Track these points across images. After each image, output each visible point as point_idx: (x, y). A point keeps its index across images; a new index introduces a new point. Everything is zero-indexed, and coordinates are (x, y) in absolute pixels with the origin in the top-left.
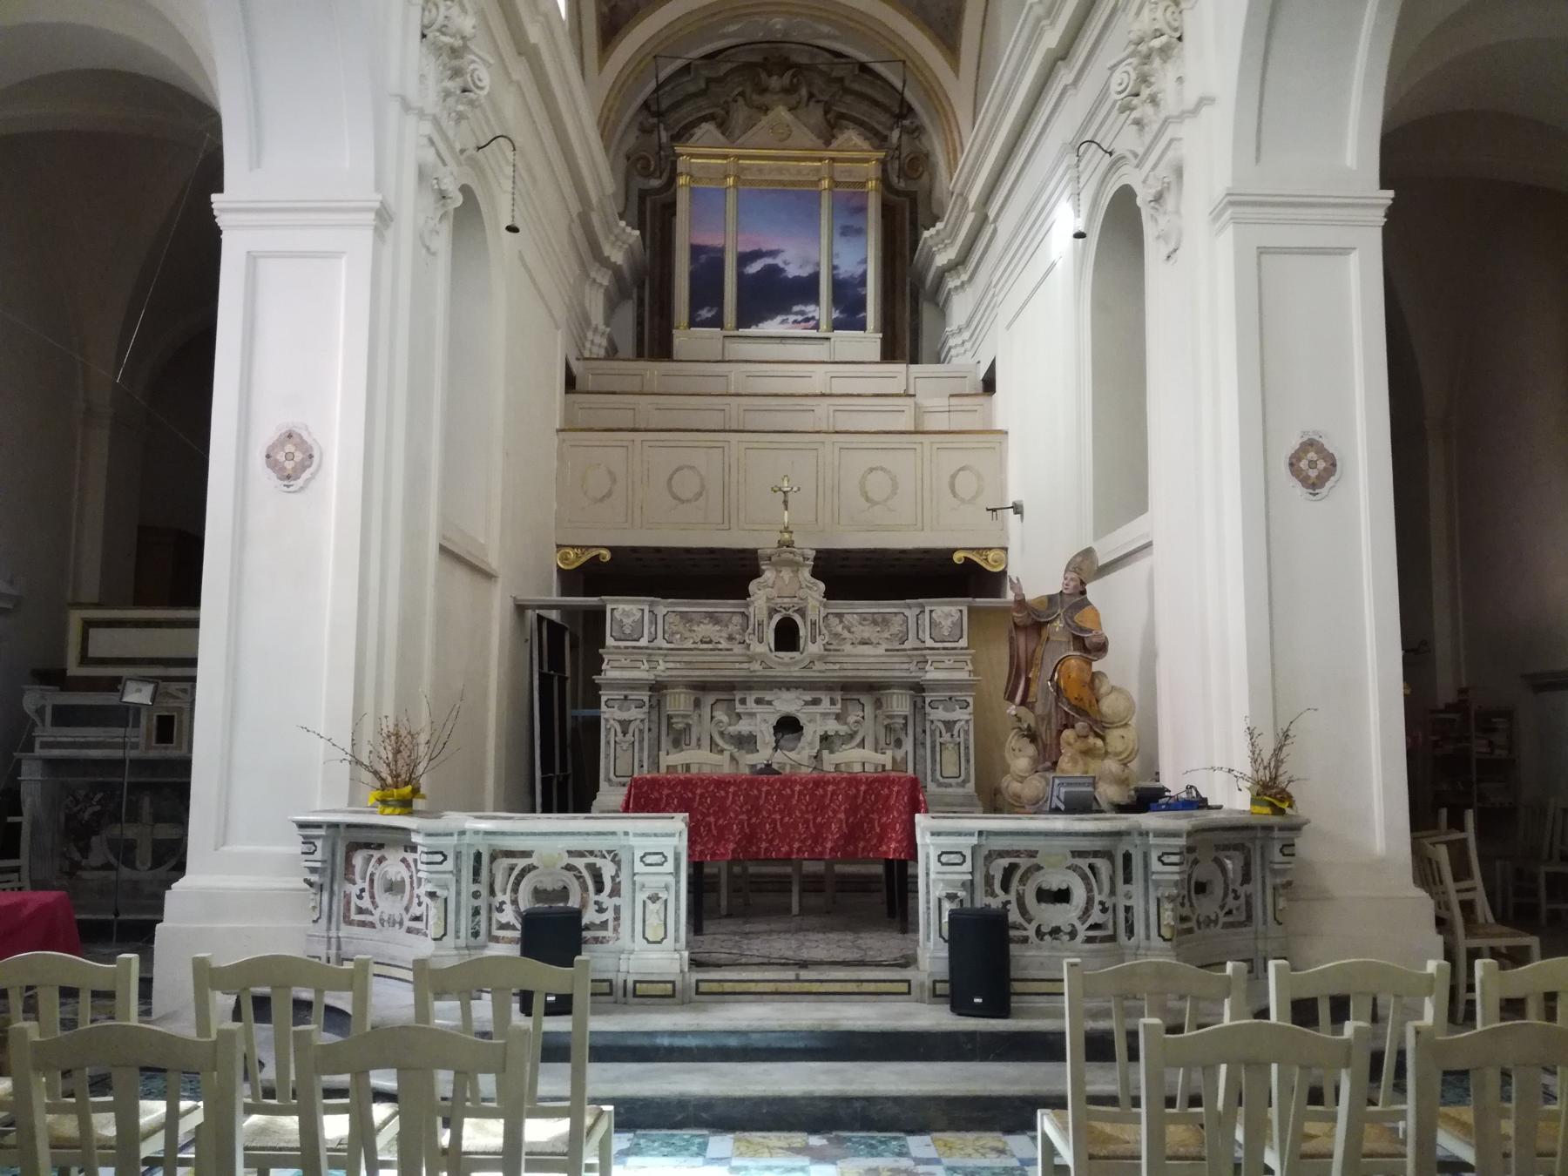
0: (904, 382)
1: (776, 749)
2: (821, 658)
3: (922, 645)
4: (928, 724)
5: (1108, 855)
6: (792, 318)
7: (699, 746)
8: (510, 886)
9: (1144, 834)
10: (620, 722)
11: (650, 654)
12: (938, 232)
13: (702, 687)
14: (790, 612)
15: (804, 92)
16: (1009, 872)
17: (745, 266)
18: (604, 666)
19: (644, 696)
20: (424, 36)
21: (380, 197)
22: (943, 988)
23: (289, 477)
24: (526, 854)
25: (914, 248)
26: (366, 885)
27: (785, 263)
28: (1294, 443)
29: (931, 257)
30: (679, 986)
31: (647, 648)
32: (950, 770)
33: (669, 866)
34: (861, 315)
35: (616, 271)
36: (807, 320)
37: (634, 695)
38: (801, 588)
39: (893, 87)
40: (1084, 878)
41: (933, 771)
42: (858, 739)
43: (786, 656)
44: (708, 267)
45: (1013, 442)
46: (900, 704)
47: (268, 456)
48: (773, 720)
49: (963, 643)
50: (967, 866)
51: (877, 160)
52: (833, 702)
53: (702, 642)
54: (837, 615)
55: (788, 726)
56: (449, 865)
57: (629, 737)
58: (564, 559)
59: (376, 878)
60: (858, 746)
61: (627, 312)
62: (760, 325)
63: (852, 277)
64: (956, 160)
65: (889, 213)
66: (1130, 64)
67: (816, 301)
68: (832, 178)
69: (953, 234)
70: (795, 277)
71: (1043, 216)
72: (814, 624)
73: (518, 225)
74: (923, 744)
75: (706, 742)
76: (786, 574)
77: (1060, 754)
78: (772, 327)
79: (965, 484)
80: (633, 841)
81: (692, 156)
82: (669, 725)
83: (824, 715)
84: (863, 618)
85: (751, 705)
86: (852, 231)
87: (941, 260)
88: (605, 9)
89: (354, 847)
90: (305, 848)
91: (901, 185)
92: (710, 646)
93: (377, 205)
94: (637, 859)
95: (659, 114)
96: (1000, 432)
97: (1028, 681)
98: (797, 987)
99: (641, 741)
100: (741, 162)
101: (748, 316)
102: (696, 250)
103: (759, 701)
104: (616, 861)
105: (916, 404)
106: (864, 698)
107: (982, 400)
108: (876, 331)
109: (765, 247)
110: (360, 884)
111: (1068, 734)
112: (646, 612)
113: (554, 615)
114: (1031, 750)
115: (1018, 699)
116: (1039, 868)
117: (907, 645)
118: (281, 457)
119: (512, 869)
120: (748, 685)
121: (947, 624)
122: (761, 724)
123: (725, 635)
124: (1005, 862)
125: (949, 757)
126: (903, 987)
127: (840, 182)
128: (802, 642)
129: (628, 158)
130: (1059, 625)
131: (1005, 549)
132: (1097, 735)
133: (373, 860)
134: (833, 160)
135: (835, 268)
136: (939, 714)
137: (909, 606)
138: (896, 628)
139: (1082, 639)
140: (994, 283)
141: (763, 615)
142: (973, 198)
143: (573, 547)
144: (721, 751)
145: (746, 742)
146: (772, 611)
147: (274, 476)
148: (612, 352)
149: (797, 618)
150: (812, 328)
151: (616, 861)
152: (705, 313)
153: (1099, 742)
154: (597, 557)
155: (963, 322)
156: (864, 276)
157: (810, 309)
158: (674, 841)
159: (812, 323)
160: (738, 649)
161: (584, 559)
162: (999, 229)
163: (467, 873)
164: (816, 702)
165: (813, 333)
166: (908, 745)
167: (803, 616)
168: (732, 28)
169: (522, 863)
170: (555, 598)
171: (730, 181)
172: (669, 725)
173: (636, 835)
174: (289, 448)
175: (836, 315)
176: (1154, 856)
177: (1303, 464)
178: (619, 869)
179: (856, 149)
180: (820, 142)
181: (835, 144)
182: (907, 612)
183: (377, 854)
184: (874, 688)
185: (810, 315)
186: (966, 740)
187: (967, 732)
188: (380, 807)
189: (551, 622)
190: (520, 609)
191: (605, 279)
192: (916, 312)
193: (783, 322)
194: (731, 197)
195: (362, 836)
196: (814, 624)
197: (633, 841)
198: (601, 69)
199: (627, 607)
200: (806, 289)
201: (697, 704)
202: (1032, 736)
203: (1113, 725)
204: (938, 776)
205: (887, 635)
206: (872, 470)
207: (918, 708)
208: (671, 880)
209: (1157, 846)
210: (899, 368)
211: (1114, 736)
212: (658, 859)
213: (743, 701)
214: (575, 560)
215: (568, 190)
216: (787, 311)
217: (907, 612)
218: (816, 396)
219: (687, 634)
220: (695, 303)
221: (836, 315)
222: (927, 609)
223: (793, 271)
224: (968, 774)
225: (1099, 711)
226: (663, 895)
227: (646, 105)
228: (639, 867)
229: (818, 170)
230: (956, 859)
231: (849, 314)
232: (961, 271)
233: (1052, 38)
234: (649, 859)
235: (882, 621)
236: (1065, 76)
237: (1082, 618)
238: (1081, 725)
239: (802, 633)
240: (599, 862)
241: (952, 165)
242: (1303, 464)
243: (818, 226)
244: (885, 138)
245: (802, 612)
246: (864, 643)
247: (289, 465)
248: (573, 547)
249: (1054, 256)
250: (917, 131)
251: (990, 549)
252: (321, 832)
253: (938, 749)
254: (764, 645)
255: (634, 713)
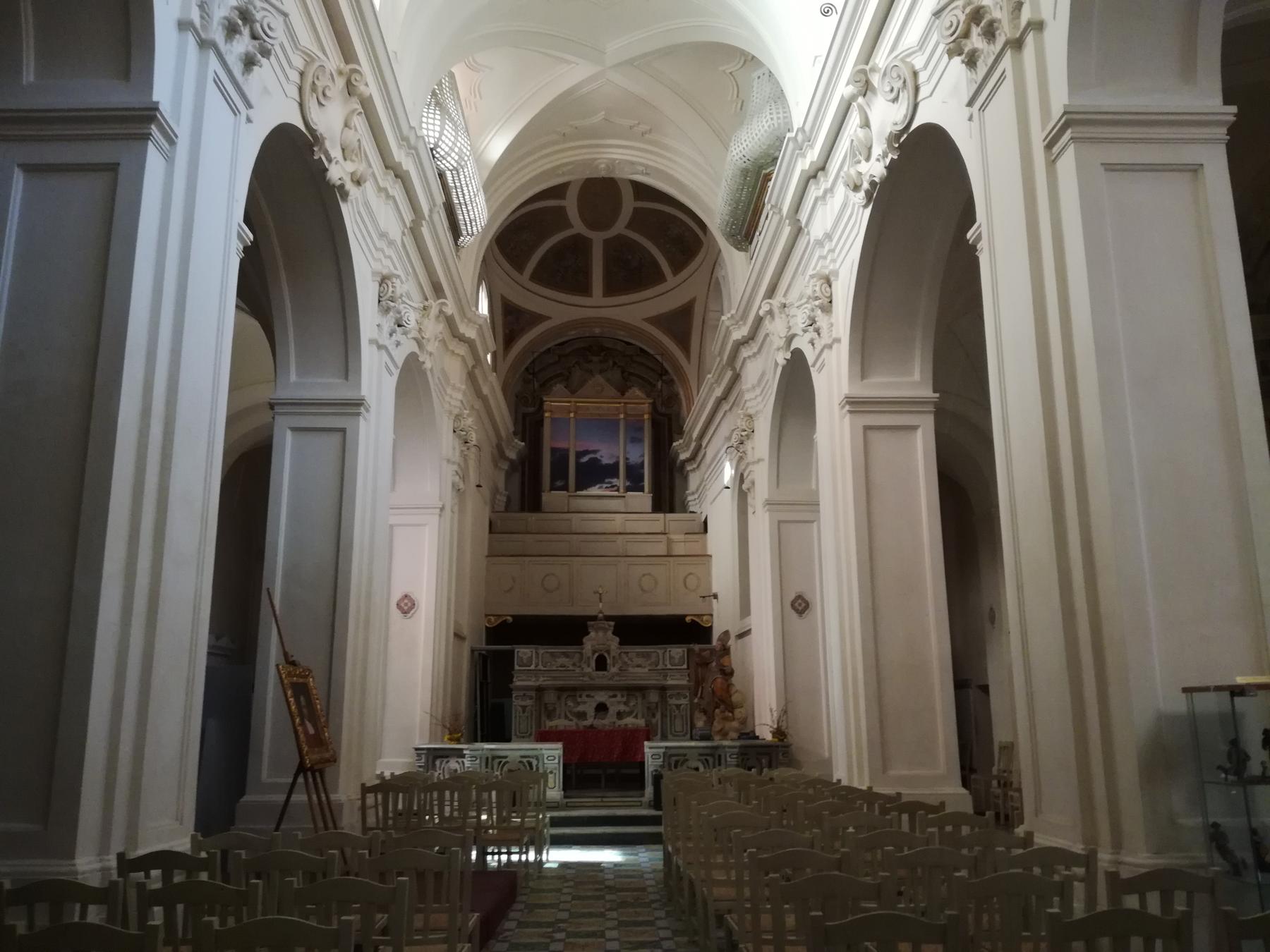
0: (663, 525)
1: (595, 718)
2: (617, 674)
3: (664, 668)
4: (668, 708)
5: (712, 755)
6: (605, 485)
7: (559, 718)
8: (500, 769)
9: (724, 747)
10: (522, 706)
11: (536, 673)
12: (680, 444)
13: (561, 690)
14: (603, 652)
15: (611, 363)
16: (677, 762)
17: (580, 458)
18: (514, 680)
19: (533, 694)
20: (454, 431)
21: (442, 503)
22: (652, 803)
23: (405, 613)
24: (506, 757)
25: (670, 449)
26: (441, 771)
27: (601, 457)
28: (793, 596)
29: (677, 455)
30: (560, 804)
31: (535, 670)
32: (679, 728)
33: (556, 761)
34: (642, 484)
35: (511, 461)
36: (613, 486)
37: (529, 693)
38: (608, 640)
39: (658, 361)
40: (703, 764)
41: (671, 729)
42: (634, 714)
43: (601, 673)
44: (560, 458)
45: (714, 560)
46: (654, 697)
47: (397, 605)
48: (594, 705)
49: (685, 666)
50: (661, 760)
51: (649, 403)
52: (622, 696)
53: (561, 667)
54: (625, 653)
55: (602, 708)
56: (478, 762)
57: (526, 714)
58: (489, 621)
59: (445, 769)
60: (634, 717)
61: (517, 478)
62: (588, 489)
63: (636, 464)
64: (691, 409)
65: (655, 424)
66: (806, 308)
67: (618, 477)
68: (626, 413)
69: (688, 445)
70: (606, 464)
71: (719, 463)
72: (614, 657)
73: (482, 484)
74: (666, 716)
75: (563, 715)
76: (601, 634)
77: (714, 719)
78: (594, 491)
79: (692, 582)
80: (544, 752)
81: (551, 402)
82: (546, 708)
83: (619, 702)
84: (638, 654)
85: (584, 698)
86: (636, 440)
87: (683, 456)
88: (507, 331)
89: (436, 758)
90: (417, 758)
91: (663, 410)
92: (564, 669)
93: (441, 506)
94: (545, 758)
95: (534, 374)
96: (708, 555)
97: (702, 687)
98: (601, 804)
99: (532, 714)
100: (578, 404)
101: (581, 485)
102: (554, 450)
103: (588, 696)
104: (537, 759)
105: (668, 538)
106: (638, 694)
107: (703, 535)
108: (649, 493)
109: (591, 449)
110: (439, 772)
111: (717, 711)
112: (534, 652)
113: (484, 652)
114: (704, 718)
115: (699, 695)
116: (687, 760)
117: (659, 667)
118: (402, 605)
119: (501, 762)
120: (583, 688)
121: (677, 657)
122: (589, 707)
123: (572, 663)
124: (674, 759)
125: (678, 723)
126: (639, 804)
127: (630, 415)
128: (608, 667)
129: (517, 397)
130: (714, 664)
131: (712, 615)
132: (729, 711)
133: (444, 762)
134: (625, 403)
135: (627, 459)
136: (673, 701)
137: (660, 649)
138: (653, 659)
139: (724, 670)
140: (706, 478)
141: (590, 654)
142: (695, 435)
143: (494, 616)
144: (571, 720)
145: (582, 716)
146: (594, 652)
147: (399, 612)
148: (507, 509)
149: (606, 655)
150: (616, 491)
151: (537, 759)
152: (559, 483)
153: (730, 714)
154: (505, 620)
155: (755, 382)
156: (643, 463)
157: (615, 481)
158: (558, 752)
159: (616, 488)
160: (578, 670)
161: (499, 622)
162: (707, 452)
163: (483, 764)
164: (615, 696)
165: (616, 493)
166: (658, 716)
167: (609, 654)
168: (573, 332)
169: (504, 760)
170: (484, 646)
171: (572, 415)
172: (546, 708)
173: (546, 749)
174: (406, 601)
175: (628, 484)
176: (728, 756)
177: (796, 605)
178: (538, 762)
179: (637, 397)
180: (619, 394)
181: (627, 394)
182: (658, 651)
183: (446, 760)
184: (641, 690)
185: (614, 484)
186: (686, 714)
187: (686, 710)
188: (449, 742)
189: (483, 655)
190: (473, 651)
191: (505, 466)
192: (672, 479)
193: (600, 488)
194: (572, 423)
195: (441, 753)
196: (614, 657)
197: (544, 752)
198: (504, 359)
199: (525, 650)
200: (612, 471)
201: (559, 698)
202: (705, 712)
203: (737, 707)
204: (673, 732)
205: (649, 662)
206: (644, 575)
207: (663, 698)
208: (557, 765)
209: (729, 752)
210: (660, 516)
211: (737, 712)
212: (552, 758)
213: (580, 696)
214: (495, 622)
215: (491, 433)
216: (602, 482)
217: (658, 651)
218: (616, 534)
219: (553, 663)
220: (554, 478)
221: (628, 484)
222: (668, 650)
223: (606, 461)
224: (687, 730)
225: (731, 701)
226: (554, 771)
227: (527, 369)
228: (546, 761)
229: (617, 408)
230: (657, 757)
231: (635, 483)
232: (822, 179)
233: (718, 392)
234: (549, 758)
235: (646, 656)
236: (726, 407)
237: (725, 661)
238: (722, 707)
239: (608, 661)
240: (531, 760)
241: (689, 410)
242: (796, 605)
243: (619, 445)
244: (655, 386)
245: (608, 652)
246: (639, 666)
247: (406, 608)
248: (494, 616)
249: (596, 697)
250: (671, 382)
251: (704, 615)
252: (425, 752)
253: (673, 718)
254: (590, 669)
255: (528, 702)
